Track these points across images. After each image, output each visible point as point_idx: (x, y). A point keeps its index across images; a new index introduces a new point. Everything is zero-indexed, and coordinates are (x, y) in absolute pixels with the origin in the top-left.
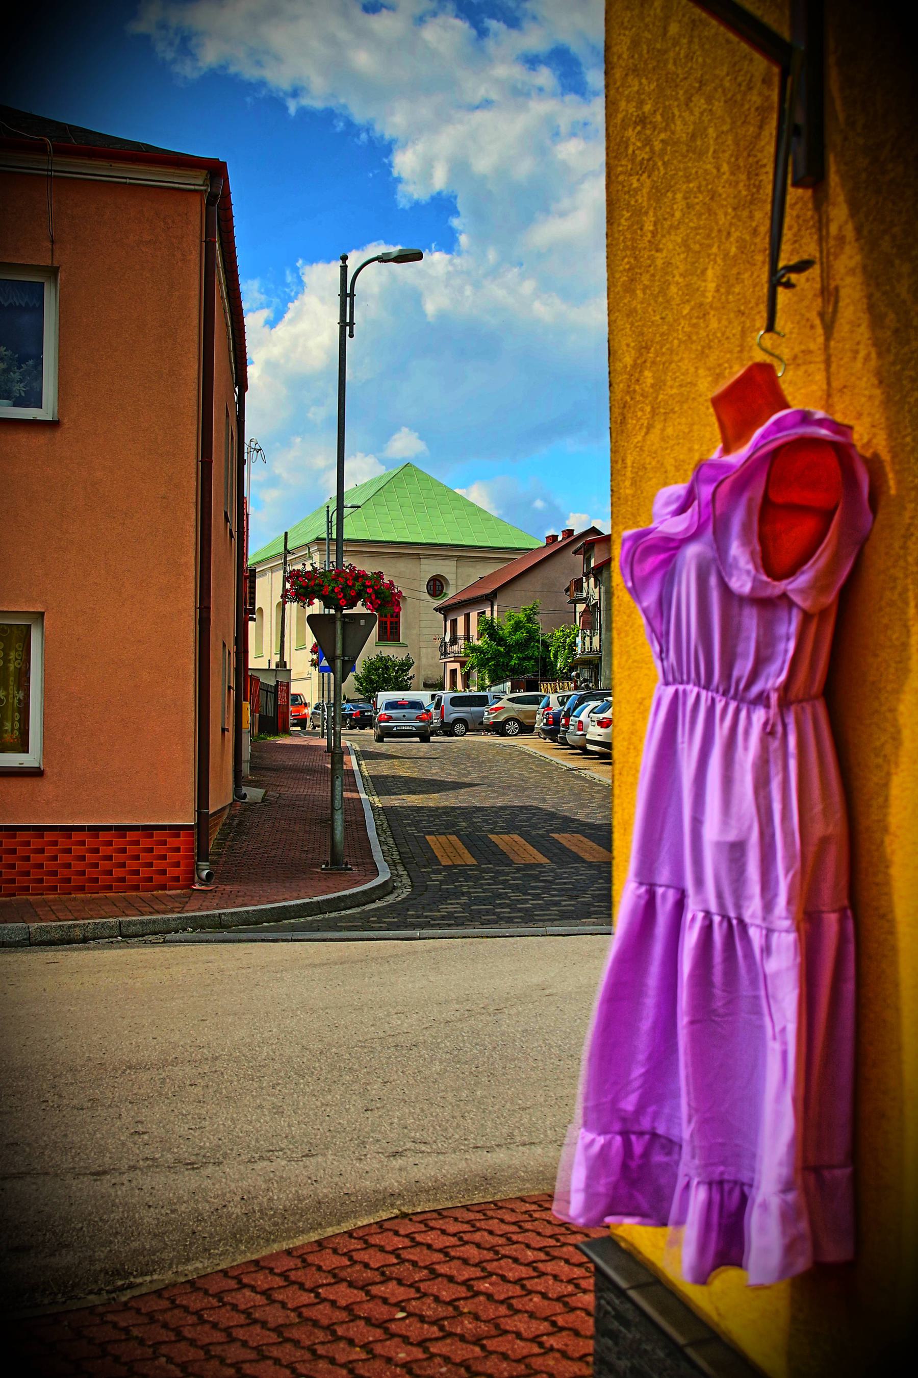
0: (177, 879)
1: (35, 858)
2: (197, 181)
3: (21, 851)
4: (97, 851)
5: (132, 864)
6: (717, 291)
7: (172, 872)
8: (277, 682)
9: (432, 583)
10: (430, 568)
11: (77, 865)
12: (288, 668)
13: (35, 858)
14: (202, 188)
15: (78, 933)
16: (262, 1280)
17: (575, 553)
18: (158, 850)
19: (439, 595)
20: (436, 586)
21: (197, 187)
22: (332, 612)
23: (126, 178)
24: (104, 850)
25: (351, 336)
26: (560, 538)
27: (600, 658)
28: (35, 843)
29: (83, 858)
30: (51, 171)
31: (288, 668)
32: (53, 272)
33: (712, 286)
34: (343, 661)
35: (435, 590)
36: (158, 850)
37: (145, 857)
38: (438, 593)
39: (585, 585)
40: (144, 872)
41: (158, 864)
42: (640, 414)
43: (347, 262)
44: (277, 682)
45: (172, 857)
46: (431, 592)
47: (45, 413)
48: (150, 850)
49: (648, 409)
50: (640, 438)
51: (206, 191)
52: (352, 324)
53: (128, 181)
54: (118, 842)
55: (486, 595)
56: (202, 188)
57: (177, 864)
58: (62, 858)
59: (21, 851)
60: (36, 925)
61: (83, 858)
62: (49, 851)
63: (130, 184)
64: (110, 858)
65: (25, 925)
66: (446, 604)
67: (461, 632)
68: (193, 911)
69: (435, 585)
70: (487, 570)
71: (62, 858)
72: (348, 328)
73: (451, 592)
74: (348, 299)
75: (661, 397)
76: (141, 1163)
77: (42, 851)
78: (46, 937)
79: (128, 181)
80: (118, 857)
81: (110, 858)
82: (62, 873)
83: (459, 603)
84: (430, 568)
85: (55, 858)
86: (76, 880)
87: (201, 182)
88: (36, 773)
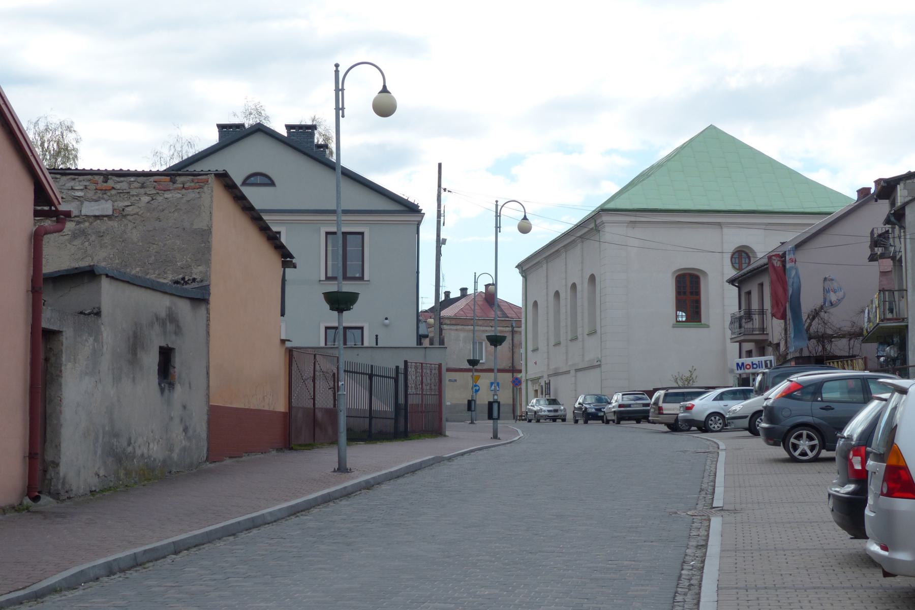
9: (736, 256)
26: (872, 191)
27: (907, 326)
46: (737, 266)
69: (740, 257)
84: (735, 238)
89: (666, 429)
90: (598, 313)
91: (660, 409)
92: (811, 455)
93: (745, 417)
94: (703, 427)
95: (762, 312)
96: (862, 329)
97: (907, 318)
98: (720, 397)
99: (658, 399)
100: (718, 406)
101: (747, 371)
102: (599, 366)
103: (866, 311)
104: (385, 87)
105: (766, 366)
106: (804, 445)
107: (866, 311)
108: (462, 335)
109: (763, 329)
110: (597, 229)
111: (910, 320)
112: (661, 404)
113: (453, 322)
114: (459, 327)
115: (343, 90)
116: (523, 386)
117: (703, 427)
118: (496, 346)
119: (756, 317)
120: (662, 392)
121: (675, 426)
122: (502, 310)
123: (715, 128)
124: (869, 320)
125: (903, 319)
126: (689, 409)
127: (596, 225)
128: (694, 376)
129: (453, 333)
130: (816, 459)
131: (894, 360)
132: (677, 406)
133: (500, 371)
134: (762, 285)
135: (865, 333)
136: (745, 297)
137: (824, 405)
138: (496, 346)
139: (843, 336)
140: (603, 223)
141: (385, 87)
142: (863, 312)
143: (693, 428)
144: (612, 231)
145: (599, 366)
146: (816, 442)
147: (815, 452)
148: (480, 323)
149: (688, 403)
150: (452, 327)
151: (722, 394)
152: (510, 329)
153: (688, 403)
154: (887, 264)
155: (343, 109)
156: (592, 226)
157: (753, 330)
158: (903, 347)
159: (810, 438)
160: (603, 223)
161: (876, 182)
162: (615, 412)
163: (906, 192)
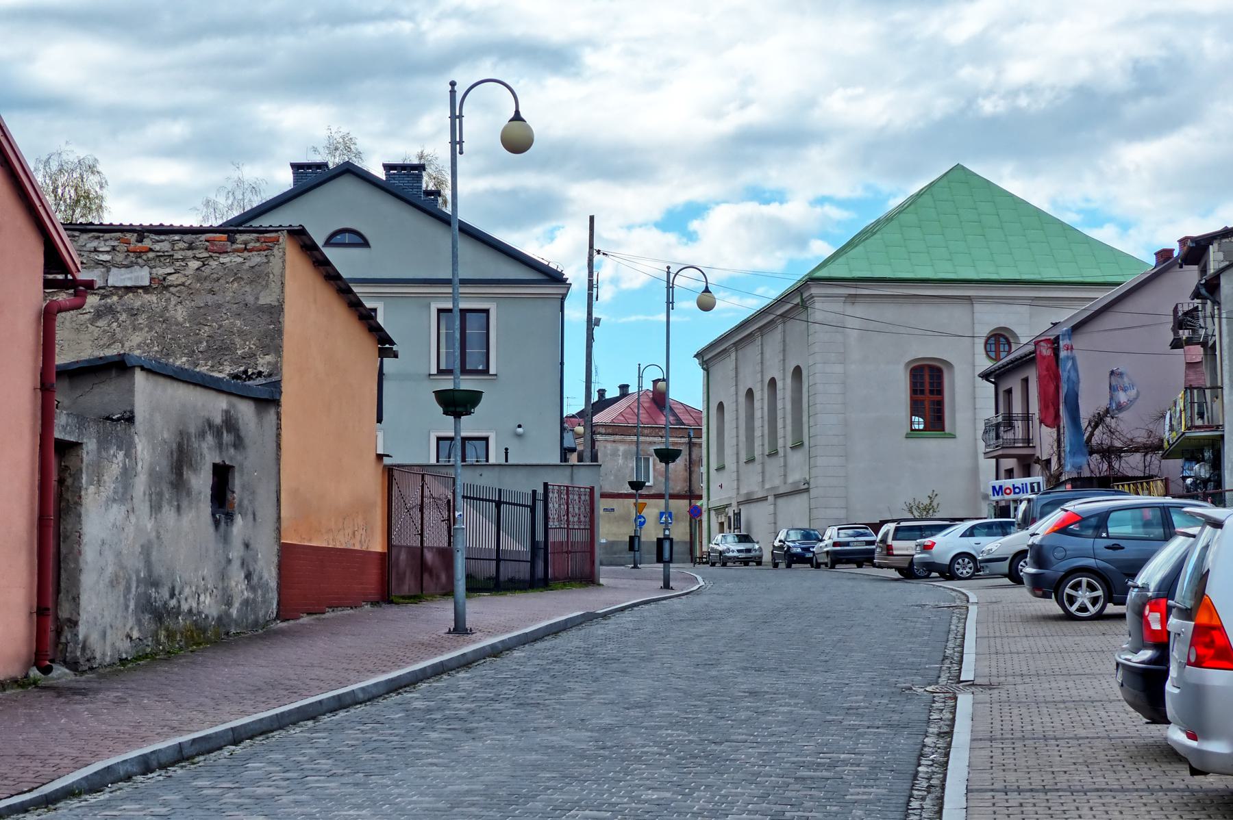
26: (1176, 254)
27: (1222, 437)
46: (993, 355)
67: (1017, 409)
69: (997, 344)
84: (990, 318)
89: (897, 575)
91: (890, 548)
94: (948, 572)
95: (1027, 418)
98: (970, 533)
100: (968, 545)
101: (1007, 497)
102: (807, 490)
104: (517, 112)
105: (1033, 490)
108: (622, 448)
109: (1027, 441)
110: (804, 306)
111: (1227, 428)
112: (890, 541)
113: (610, 431)
114: (618, 437)
115: (461, 116)
116: (705, 517)
117: (948, 572)
118: (667, 463)
119: (1019, 425)
120: (892, 526)
121: (909, 572)
122: (675, 415)
124: (1172, 429)
125: (1218, 427)
126: (927, 548)
127: (802, 300)
128: (935, 504)
129: (609, 446)
130: (1100, 617)
131: (1205, 482)
132: (912, 544)
133: (673, 497)
134: (1026, 381)
137: (1110, 542)
139: (1137, 450)
141: (517, 112)
143: (934, 574)
144: (823, 308)
145: (807, 490)
146: (1100, 593)
147: (1098, 607)
148: (646, 431)
149: (927, 541)
150: (607, 437)
151: (973, 527)
152: (686, 440)
153: (927, 541)
154: (1197, 353)
155: (461, 142)
156: (797, 300)
157: (1015, 441)
158: (1217, 464)
159: (1092, 588)
161: (1180, 241)
162: (827, 552)
163: (1221, 256)
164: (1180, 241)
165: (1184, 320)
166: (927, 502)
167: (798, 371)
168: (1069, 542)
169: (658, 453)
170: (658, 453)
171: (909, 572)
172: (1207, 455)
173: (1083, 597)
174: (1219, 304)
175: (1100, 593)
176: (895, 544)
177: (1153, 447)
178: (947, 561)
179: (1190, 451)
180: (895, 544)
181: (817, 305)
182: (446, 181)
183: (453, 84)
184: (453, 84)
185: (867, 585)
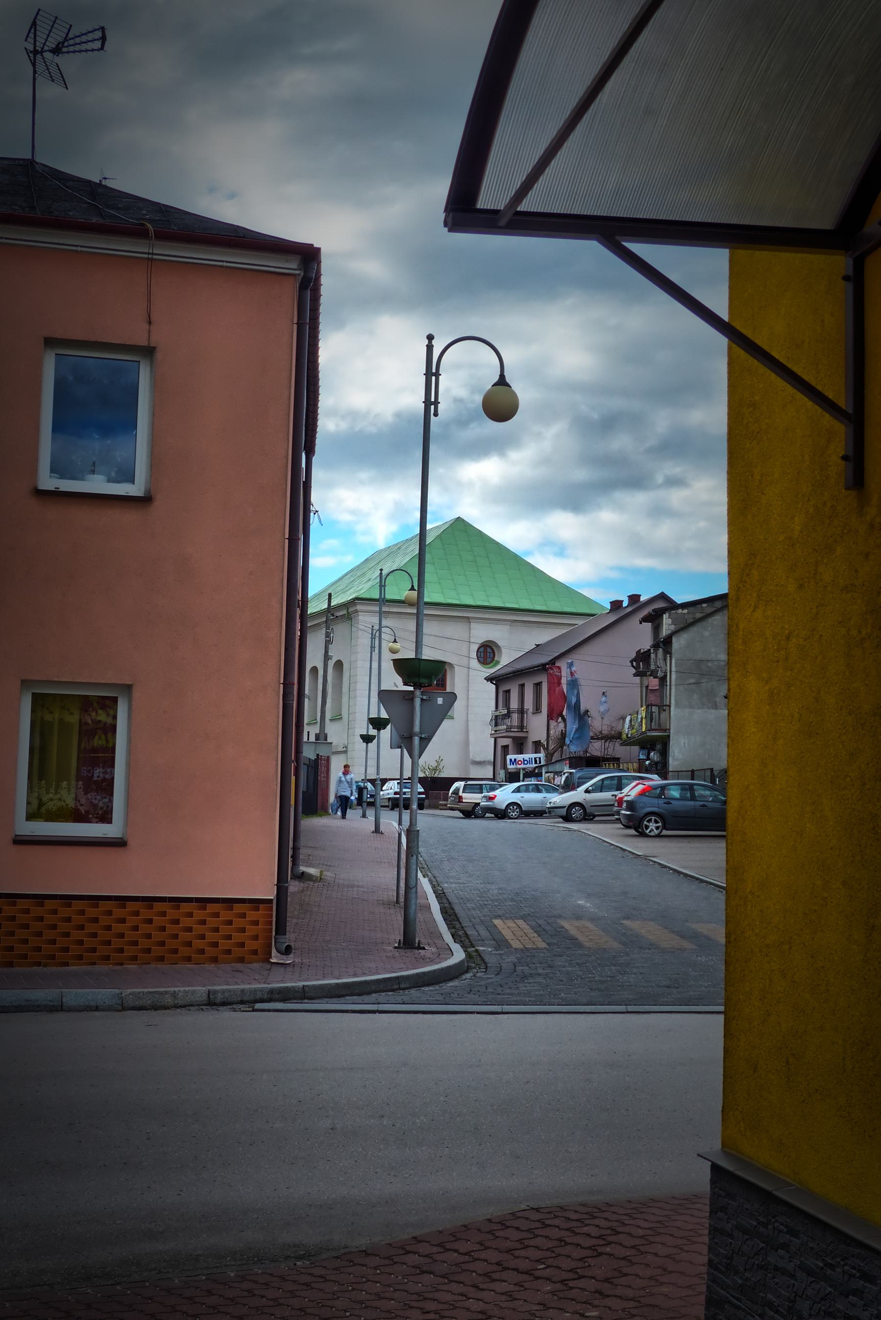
0: (255, 952)
1: (118, 928)
2: (292, 265)
3: (104, 920)
4: (177, 922)
5: (211, 937)
6: (801, 532)
7: (251, 945)
8: (318, 755)
9: (482, 650)
10: (482, 633)
11: (157, 936)
12: (329, 741)
13: (118, 928)
14: (297, 272)
15: (169, 1000)
16: (424, 1248)
17: (645, 620)
18: (238, 923)
19: (492, 662)
20: (487, 652)
21: (291, 271)
22: (411, 689)
23: (222, 261)
24: (185, 922)
25: (436, 415)
26: (625, 604)
27: (669, 736)
28: (118, 912)
29: (163, 929)
30: (153, 254)
31: (329, 741)
32: (148, 352)
33: (798, 528)
34: (421, 738)
35: (485, 658)
36: (238, 923)
37: (225, 930)
38: (489, 660)
39: (653, 656)
40: (224, 944)
41: (237, 937)
42: (749, 597)
43: (434, 342)
44: (318, 755)
45: (251, 930)
46: (482, 659)
47: (134, 489)
48: (230, 923)
49: (755, 595)
50: (748, 613)
51: (299, 275)
52: (436, 403)
53: (225, 264)
54: (199, 914)
55: (544, 665)
56: (297, 272)
57: (256, 938)
58: (144, 928)
59: (104, 920)
60: (129, 991)
61: (163, 929)
62: (132, 920)
63: (226, 267)
64: (190, 929)
65: (117, 991)
66: (498, 673)
67: (514, 705)
68: (278, 982)
69: (485, 652)
70: (544, 636)
71: (144, 928)
72: (433, 407)
73: (506, 659)
74: (434, 378)
75: (764, 589)
76: (171, 1270)
77: (123, 921)
78: (138, 1003)
79: (225, 264)
80: (198, 929)
81: (190, 929)
82: (144, 943)
83: (514, 672)
84: (482, 633)
85: (136, 928)
86: (157, 951)
87: (295, 266)
88: (120, 843)
89: (461, 815)
90: (345, 699)
91: (461, 798)
92: (656, 832)
93: (564, 807)
94: (501, 814)
95: (522, 711)
96: (620, 734)
97: (669, 730)
98: (518, 790)
99: (457, 790)
100: (517, 798)
101: (519, 766)
102: (345, 752)
103: (628, 719)
105: (536, 763)
106: (652, 826)
107: (628, 719)
109: (521, 727)
111: (672, 731)
112: (461, 794)
117: (501, 814)
118: (367, 743)
119: (515, 716)
120: (463, 783)
121: (470, 812)
123: (463, 520)
124: (631, 726)
125: (665, 731)
126: (491, 799)
128: (441, 767)
130: (658, 836)
131: (656, 763)
132: (480, 796)
135: (624, 736)
136: (502, 698)
137: (666, 801)
138: (367, 743)
139: (602, 738)
140: (357, 611)
142: (624, 719)
143: (488, 815)
145: (345, 752)
146: (660, 824)
147: (659, 831)
149: (491, 794)
151: (519, 787)
153: (491, 794)
154: (654, 683)
157: (511, 727)
158: (664, 753)
159: (656, 822)
160: (357, 611)
161: (629, 597)
162: (389, 799)
163: (670, 621)
164: (629, 597)
165: (642, 658)
166: (434, 764)
167: (339, 665)
168: (645, 799)
169: (362, 736)
170: (362, 736)
171: (470, 812)
172: (658, 747)
173: (652, 826)
174: (670, 654)
175: (660, 824)
176: (464, 795)
177: (616, 736)
178: (503, 807)
179: (646, 743)
180: (464, 795)
181: (361, 618)
182: (498, 663)
183: (381, 570)
184: (381, 570)
185: (431, 819)
